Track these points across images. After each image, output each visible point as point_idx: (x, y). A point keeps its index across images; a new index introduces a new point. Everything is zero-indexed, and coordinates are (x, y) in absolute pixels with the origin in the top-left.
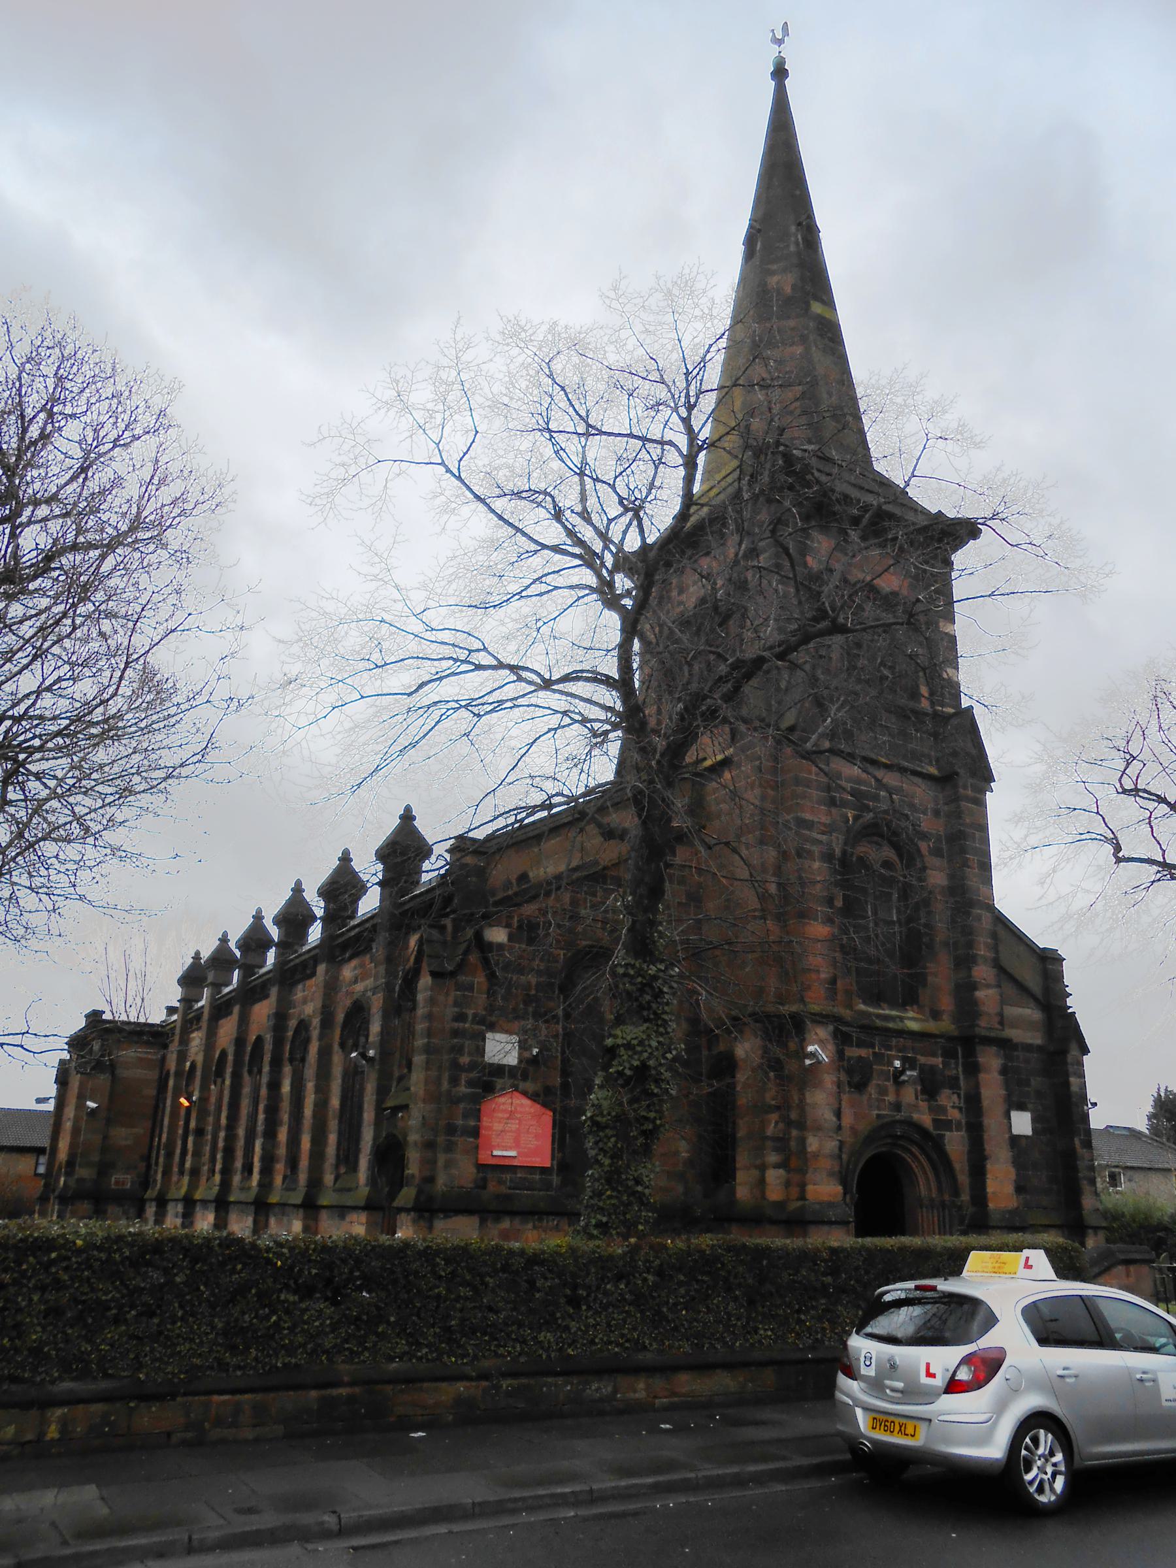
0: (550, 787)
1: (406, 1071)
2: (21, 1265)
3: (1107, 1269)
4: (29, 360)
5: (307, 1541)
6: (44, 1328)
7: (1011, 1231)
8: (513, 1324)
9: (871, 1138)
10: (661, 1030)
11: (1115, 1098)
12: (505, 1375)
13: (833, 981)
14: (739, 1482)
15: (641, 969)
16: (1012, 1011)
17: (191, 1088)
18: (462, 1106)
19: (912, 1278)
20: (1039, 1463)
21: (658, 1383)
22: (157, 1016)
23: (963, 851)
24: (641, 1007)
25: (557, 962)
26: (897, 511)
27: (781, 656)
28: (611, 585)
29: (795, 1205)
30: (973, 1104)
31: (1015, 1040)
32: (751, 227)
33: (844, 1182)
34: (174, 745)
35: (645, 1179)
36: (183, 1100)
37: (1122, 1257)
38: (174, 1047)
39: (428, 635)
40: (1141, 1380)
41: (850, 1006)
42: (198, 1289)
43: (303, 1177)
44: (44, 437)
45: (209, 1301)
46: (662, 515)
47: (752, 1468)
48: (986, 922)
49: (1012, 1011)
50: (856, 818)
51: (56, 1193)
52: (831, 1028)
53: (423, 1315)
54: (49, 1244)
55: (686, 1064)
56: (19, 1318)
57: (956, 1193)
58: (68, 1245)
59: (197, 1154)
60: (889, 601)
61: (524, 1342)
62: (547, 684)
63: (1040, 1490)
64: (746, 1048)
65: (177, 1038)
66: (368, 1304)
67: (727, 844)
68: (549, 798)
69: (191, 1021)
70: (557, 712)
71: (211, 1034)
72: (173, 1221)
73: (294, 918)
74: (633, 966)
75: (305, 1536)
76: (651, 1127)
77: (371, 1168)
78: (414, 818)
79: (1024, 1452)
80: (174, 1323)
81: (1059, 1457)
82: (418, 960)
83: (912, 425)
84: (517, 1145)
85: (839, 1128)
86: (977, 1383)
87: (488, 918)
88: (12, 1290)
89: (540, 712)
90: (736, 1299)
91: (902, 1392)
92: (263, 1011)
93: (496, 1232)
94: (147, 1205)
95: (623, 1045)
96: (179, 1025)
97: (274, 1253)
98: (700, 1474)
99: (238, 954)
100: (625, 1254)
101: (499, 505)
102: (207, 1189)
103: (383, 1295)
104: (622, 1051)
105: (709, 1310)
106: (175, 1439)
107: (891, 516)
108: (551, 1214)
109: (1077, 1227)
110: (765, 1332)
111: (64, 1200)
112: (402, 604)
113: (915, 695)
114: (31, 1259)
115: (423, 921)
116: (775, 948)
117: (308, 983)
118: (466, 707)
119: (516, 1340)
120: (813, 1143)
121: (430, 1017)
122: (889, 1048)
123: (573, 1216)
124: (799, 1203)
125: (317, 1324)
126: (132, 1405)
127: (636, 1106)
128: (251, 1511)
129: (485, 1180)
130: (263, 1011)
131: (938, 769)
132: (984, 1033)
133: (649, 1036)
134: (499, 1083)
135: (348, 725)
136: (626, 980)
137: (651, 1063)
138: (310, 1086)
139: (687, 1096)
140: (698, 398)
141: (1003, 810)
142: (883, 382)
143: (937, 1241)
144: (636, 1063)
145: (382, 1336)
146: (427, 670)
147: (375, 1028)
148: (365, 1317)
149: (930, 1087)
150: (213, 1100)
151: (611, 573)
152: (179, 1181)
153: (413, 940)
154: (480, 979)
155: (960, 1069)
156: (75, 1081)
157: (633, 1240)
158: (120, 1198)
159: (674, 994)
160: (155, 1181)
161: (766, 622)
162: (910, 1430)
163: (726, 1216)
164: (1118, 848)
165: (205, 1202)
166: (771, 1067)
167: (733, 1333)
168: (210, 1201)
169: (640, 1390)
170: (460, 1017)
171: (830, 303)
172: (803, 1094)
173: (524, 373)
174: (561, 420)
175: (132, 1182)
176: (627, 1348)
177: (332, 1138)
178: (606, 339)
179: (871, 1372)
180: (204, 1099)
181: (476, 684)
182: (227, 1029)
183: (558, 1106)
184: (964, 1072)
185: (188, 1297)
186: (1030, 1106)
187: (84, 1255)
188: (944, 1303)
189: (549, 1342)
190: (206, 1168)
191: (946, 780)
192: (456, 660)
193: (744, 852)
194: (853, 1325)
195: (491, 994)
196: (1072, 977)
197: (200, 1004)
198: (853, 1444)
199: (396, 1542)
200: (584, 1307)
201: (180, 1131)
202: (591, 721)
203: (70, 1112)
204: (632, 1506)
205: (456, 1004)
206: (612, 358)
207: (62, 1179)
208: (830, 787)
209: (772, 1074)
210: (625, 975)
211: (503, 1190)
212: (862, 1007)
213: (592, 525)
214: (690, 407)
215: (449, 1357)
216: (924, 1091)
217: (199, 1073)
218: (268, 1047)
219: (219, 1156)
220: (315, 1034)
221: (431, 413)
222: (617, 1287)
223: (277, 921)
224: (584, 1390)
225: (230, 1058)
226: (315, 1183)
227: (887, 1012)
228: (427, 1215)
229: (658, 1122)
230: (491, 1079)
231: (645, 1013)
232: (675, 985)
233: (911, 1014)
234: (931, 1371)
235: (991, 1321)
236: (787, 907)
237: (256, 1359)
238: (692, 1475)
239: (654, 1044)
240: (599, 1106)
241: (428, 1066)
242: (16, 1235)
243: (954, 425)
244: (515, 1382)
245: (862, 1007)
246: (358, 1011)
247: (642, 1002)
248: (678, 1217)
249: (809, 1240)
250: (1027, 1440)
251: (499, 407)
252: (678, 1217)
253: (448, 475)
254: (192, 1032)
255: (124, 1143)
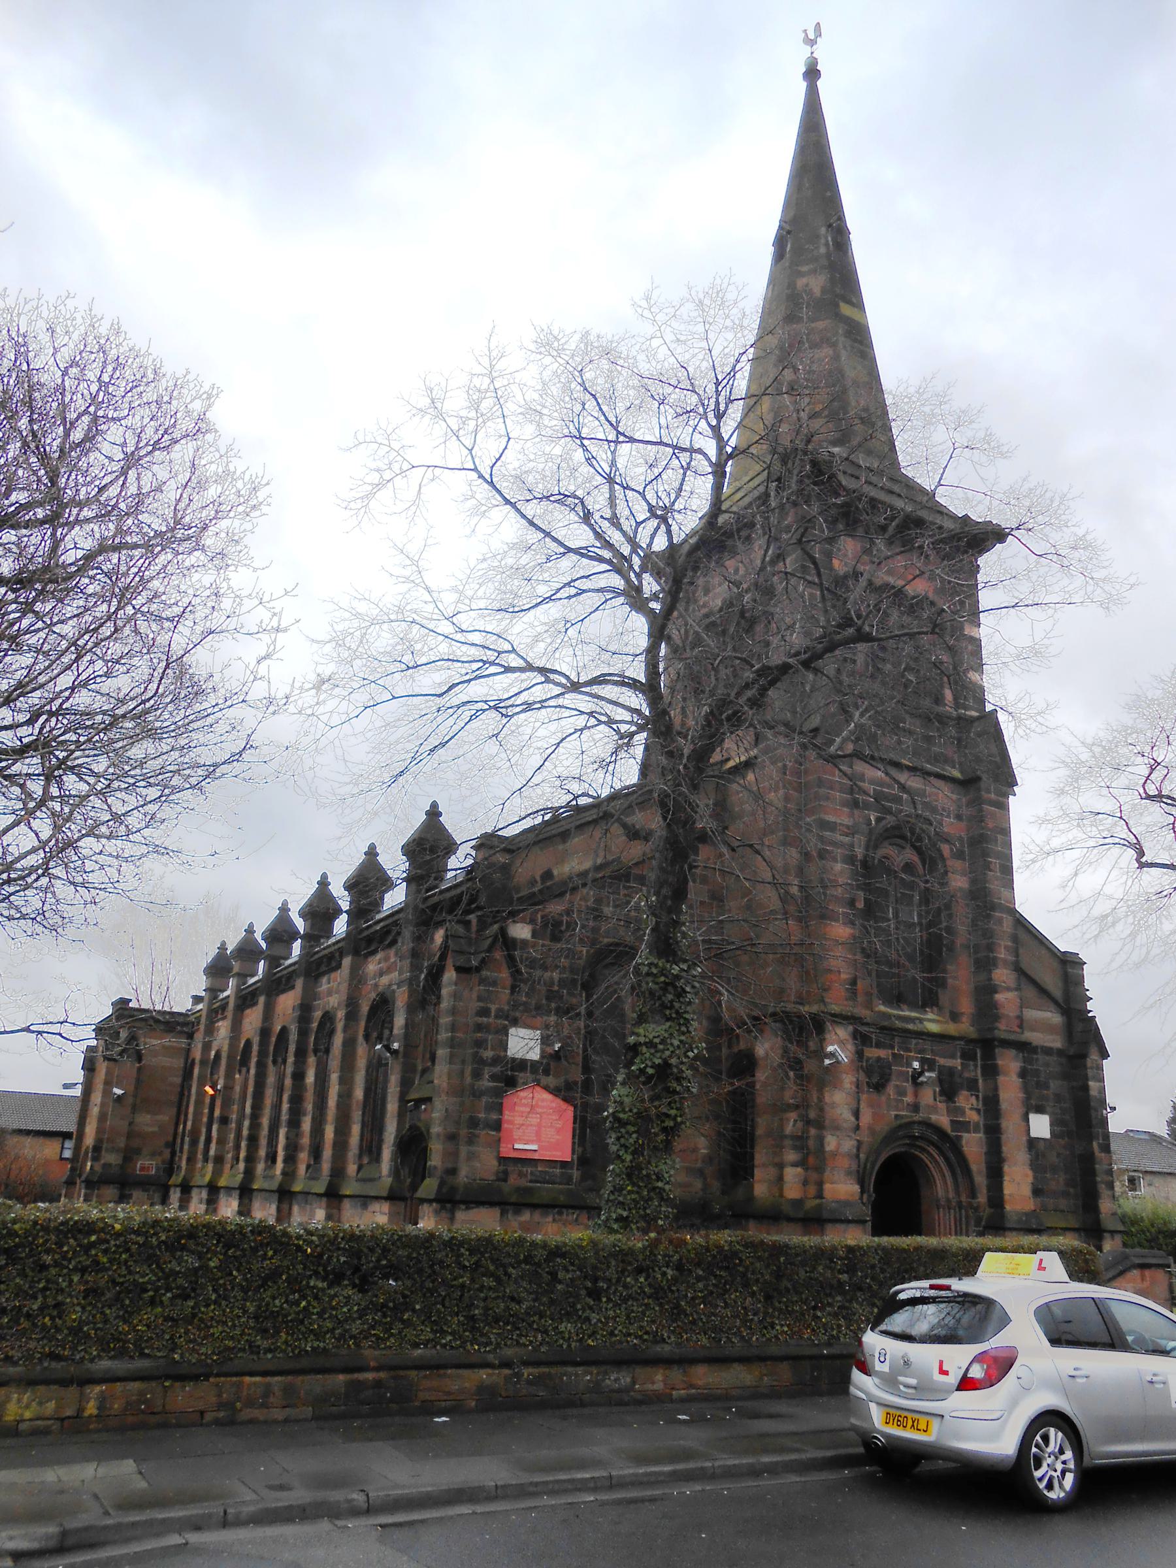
0: (576, 788)
1: (429, 1064)
2: (61, 1247)
3: (1121, 1273)
4: (73, 363)
5: (337, 1518)
6: (83, 1308)
7: (1030, 1231)
8: (535, 1314)
9: (891, 1136)
10: (684, 1029)
11: (1131, 1105)
12: (526, 1364)
13: (854, 982)
14: (755, 1472)
15: (664, 969)
16: (1031, 1014)
17: (216, 1077)
18: (484, 1099)
19: (927, 1277)
20: (1049, 1461)
21: (676, 1374)
22: (181, 1004)
23: (985, 854)
24: (664, 1006)
25: (579, 958)
26: (924, 514)
27: (806, 664)
28: (639, 589)
29: (811, 1204)
30: (992, 1107)
31: (1035, 1044)
32: (781, 228)
33: (862, 1182)
34: (210, 747)
35: (666, 1175)
36: (208, 1089)
37: (1137, 1261)
38: (199, 1037)
39: (459, 637)
40: (1151, 1382)
41: (869, 1005)
42: (231, 1274)
43: (326, 1166)
44: (89, 438)
45: (241, 1285)
46: (688, 522)
47: (766, 1459)
48: (1007, 924)
49: (1031, 1014)
50: (878, 820)
51: (83, 1178)
52: (851, 1028)
53: (447, 1304)
54: (88, 1227)
55: (706, 1062)
56: (60, 1298)
57: (973, 1193)
58: (106, 1228)
59: (221, 1141)
60: (914, 606)
61: (546, 1332)
62: (575, 687)
63: (1050, 1487)
64: (767, 1048)
65: (202, 1027)
66: (396, 1292)
67: (751, 846)
68: (575, 798)
69: (216, 1011)
70: (582, 713)
71: (236, 1027)
72: (197, 1207)
73: (321, 910)
74: (656, 966)
75: (334, 1512)
76: (672, 1124)
77: (393, 1159)
78: (440, 814)
79: (1034, 1450)
80: (207, 1306)
81: (1069, 1455)
82: (443, 957)
83: (940, 435)
84: (538, 1140)
85: (858, 1128)
86: (991, 1381)
87: (514, 916)
88: (53, 1271)
89: (567, 713)
90: (753, 1294)
91: (915, 1388)
92: (288, 1002)
93: (515, 1224)
94: (172, 1190)
95: (645, 1044)
96: (204, 1013)
97: (304, 1241)
98: (717, 1464)
99: (264, 945)
100: (645, 1248)
101: (530, 510)
102: (232, 1176)
103: (409, 1283)
104: (644, 1049)
105: (727, 1305)
106: (209, 1417)
107: (919, 523)
108: (567, 1207)
109: (1094, 1231)
110: (781, 1327)
111: (90, 1184)
112: (431, 606)
113: (938, 700)
114: (71, 1241)
115: (449, 918)
116: (796, 950)
117: (333, 975)
118: (496, 708)
119: (537, 1330)
120: (831, 1143)
121: (453, 1011)
122: (908, 1050)
123: (593, 1210)
124: (817, 1201)
125: (345, 1310)
126: (167, 1384)
127: (656, 1103)
128: (282, 1488)
129: (506, 1173)
130: (288, 1002)
131: (962, 773)
132: (1003, 1036)
133: (671, 1034)
134: (521, 1077)
135: (378, 724)
136: (650, 979)
137: (673, 1061)
138: (334, 1077)
139: (707, 1094)
140: (727, 407)
141: (1027, 816)
142: (912, 390)
143: (953, 1242)
144: (657, 1061)
145: (408, 1323)
146: (456, 673)
147: (399, 1021)
148: (391, 1305)
149: (949, 1089)
150: (238, 1089)
151: (639, 576)
152: (203, 1167)
153: (439, 936)
154: (504, 974)
155: (979, 1071)
156: (102, 1068)
157: (653, 1235)
158: (144, 1184)
159: (696, 994)
160: (179, 1167)
161: (791, 629)
162: (922, 1426)
163: (743, 1213)
164: (1141, 853)
165: (229, 1189)
166: (791, 1068)
167: (750, 1328)
168: (234, 1189)
169: (657, 1380)
170: (484, 1012)
171: (860, 306)
172: (822, 1094)
173: (557, 380)
174: (593, 428)
175: (158, 1169)
176: (646, 1340)
177: (356, 1129)
178: (637, 347)
179: (885, 1368)
180: (228, 1088)
181: (505, 685)
182: (253, 1019)
183: (579, 1102)
184: (983, 1075)
185: (221, 1282)
186: (1048, 1109)
187: (122, 1239)
188: (958, 1302)
189: (570, 1332)
190: (230, 1155)
191: (969, 783)
192: (485, 662)
193: (767, 853)
194: (868, 1321)
195: (513, 989)
196: (1091, 982)
197: (226, 994)
198: (867, 1440)
199: (422, 1521)
200: (604, 1299)
201: (205, 1120)
202: (617, 722)
203: (97, 1098)
204: (649, 1493)
205: (480, 999)
206: (644, 367)
207: (89, 1164)
208: (854, 786)
209: (791, 1074)
210: (648, 974)
211: (523, 1183)
212: (882, 1008)
213: (621, 530)
214: (720, 416)
215: (472, 1345)
216: (943, 1092)
217: (224, 1062)
218: (293, 1037)
219: (243, 1144)
220: (340, 1026)
221: (464, 421)
222: (637, 1280)
223: (303, 914)
224: (604, 1380)
225: (255, 1048)
226: (338, 1172)
227: (907, 1013)
228: (448, 1206)
229: (679, 1119)
230: (512, 1074)
231: (668, 1012)
232: (697, 985)
233: (930, 1016)
234: (944, 1368)
235: (1005, 1320)
236: (809, 908)
237: (286, 1342)
238: (708, 1464)
239: (676, 1043)
240: (621, 1103)
241: (452, 1059)
242: (56, 1218)
243: (981, 434)
244: (536, 1371)
245: (882, 1008)
246: (382, 1006)
247: (665, 1000)
248: (696, 1213)
249: (826, 1238)
250: (1038, 1438)
251: (532, 413)
252: (696, 1213)
253: (481, 481)
254: (218, 1021)
255: (150, 1129)
